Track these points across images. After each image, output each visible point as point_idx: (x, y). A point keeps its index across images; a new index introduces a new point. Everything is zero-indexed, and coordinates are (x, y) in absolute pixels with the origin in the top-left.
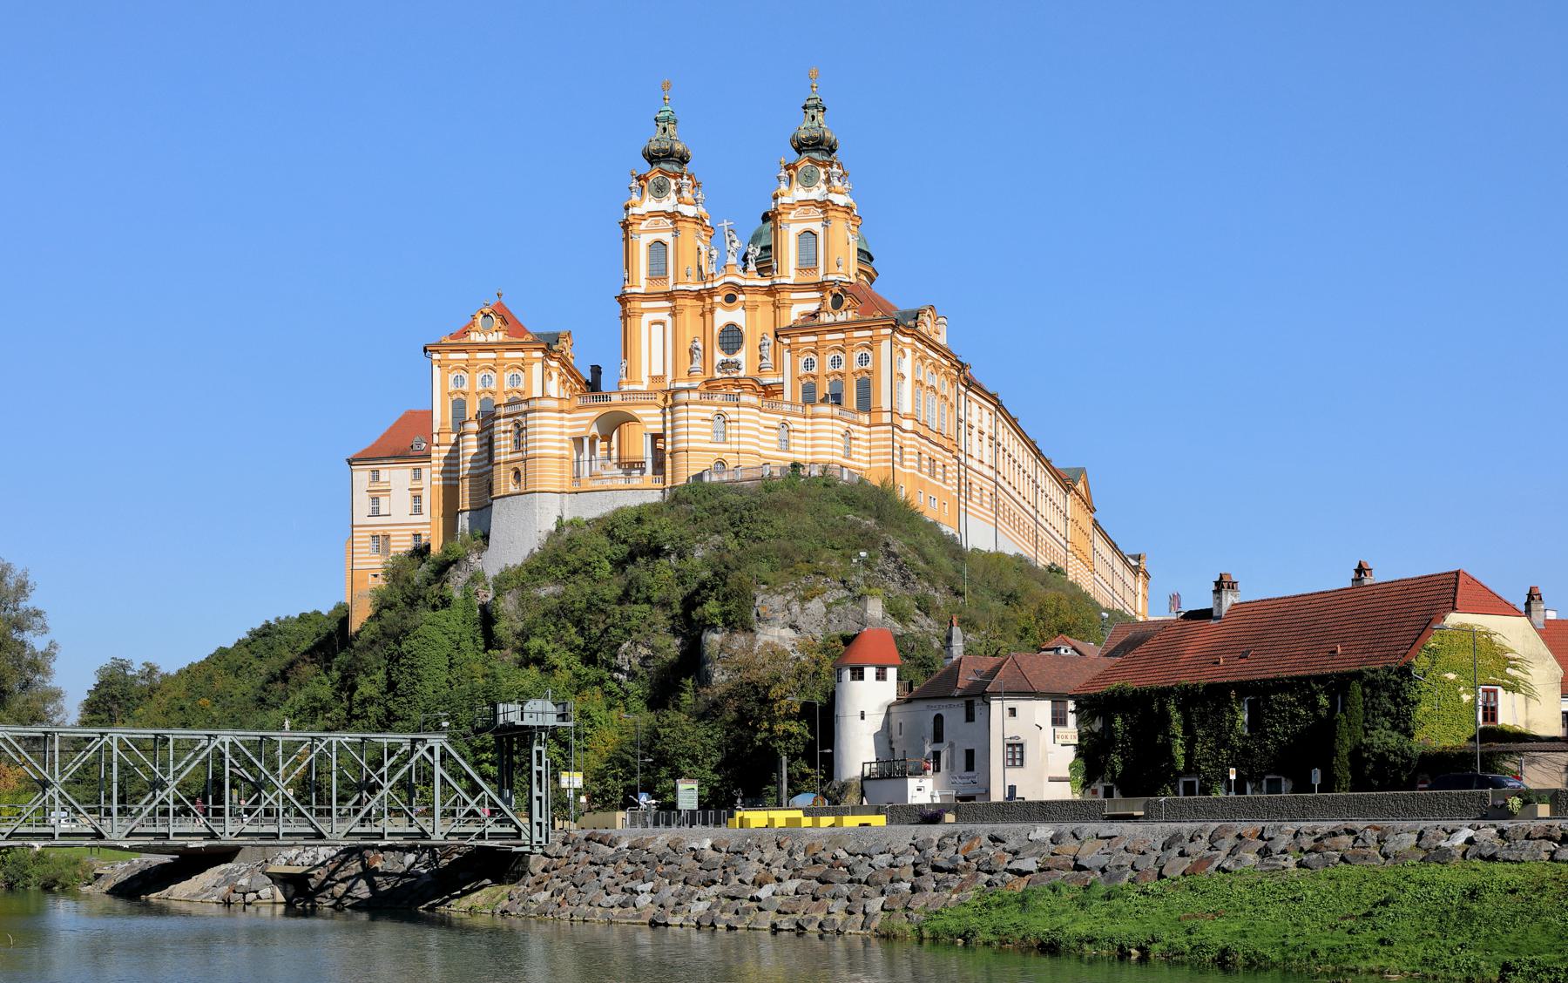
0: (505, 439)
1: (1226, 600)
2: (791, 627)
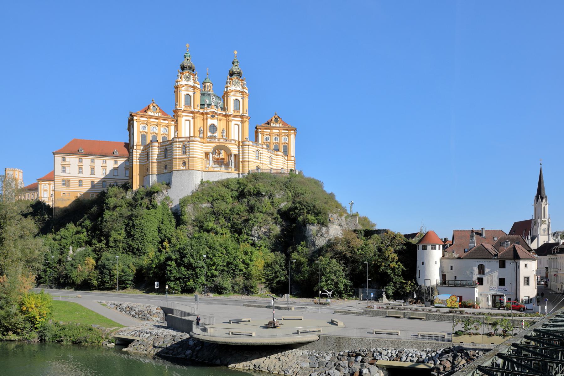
0: (179, 150)
2: (339, 225)
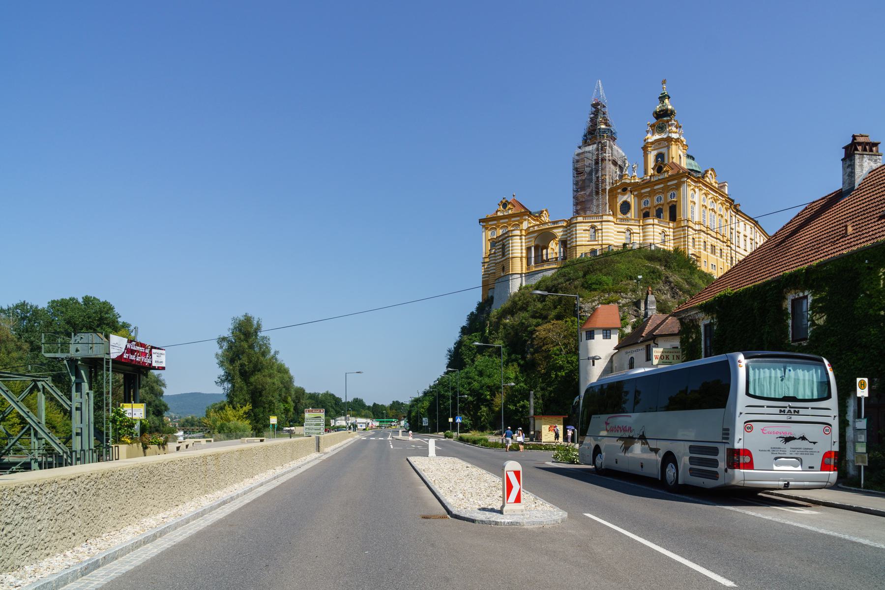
1: (861, 166)
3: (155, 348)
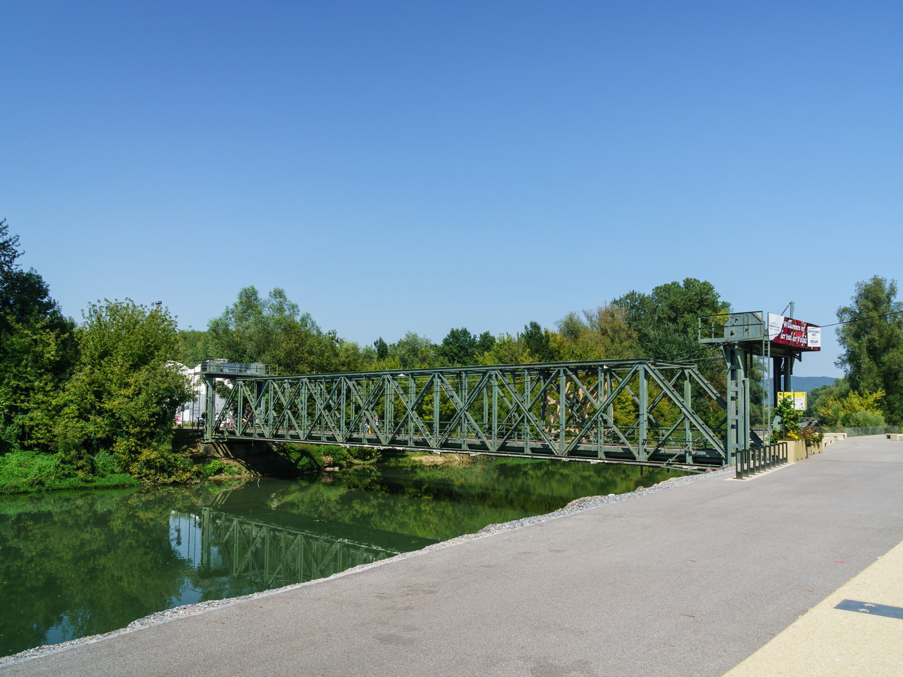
3: (811, 325)
